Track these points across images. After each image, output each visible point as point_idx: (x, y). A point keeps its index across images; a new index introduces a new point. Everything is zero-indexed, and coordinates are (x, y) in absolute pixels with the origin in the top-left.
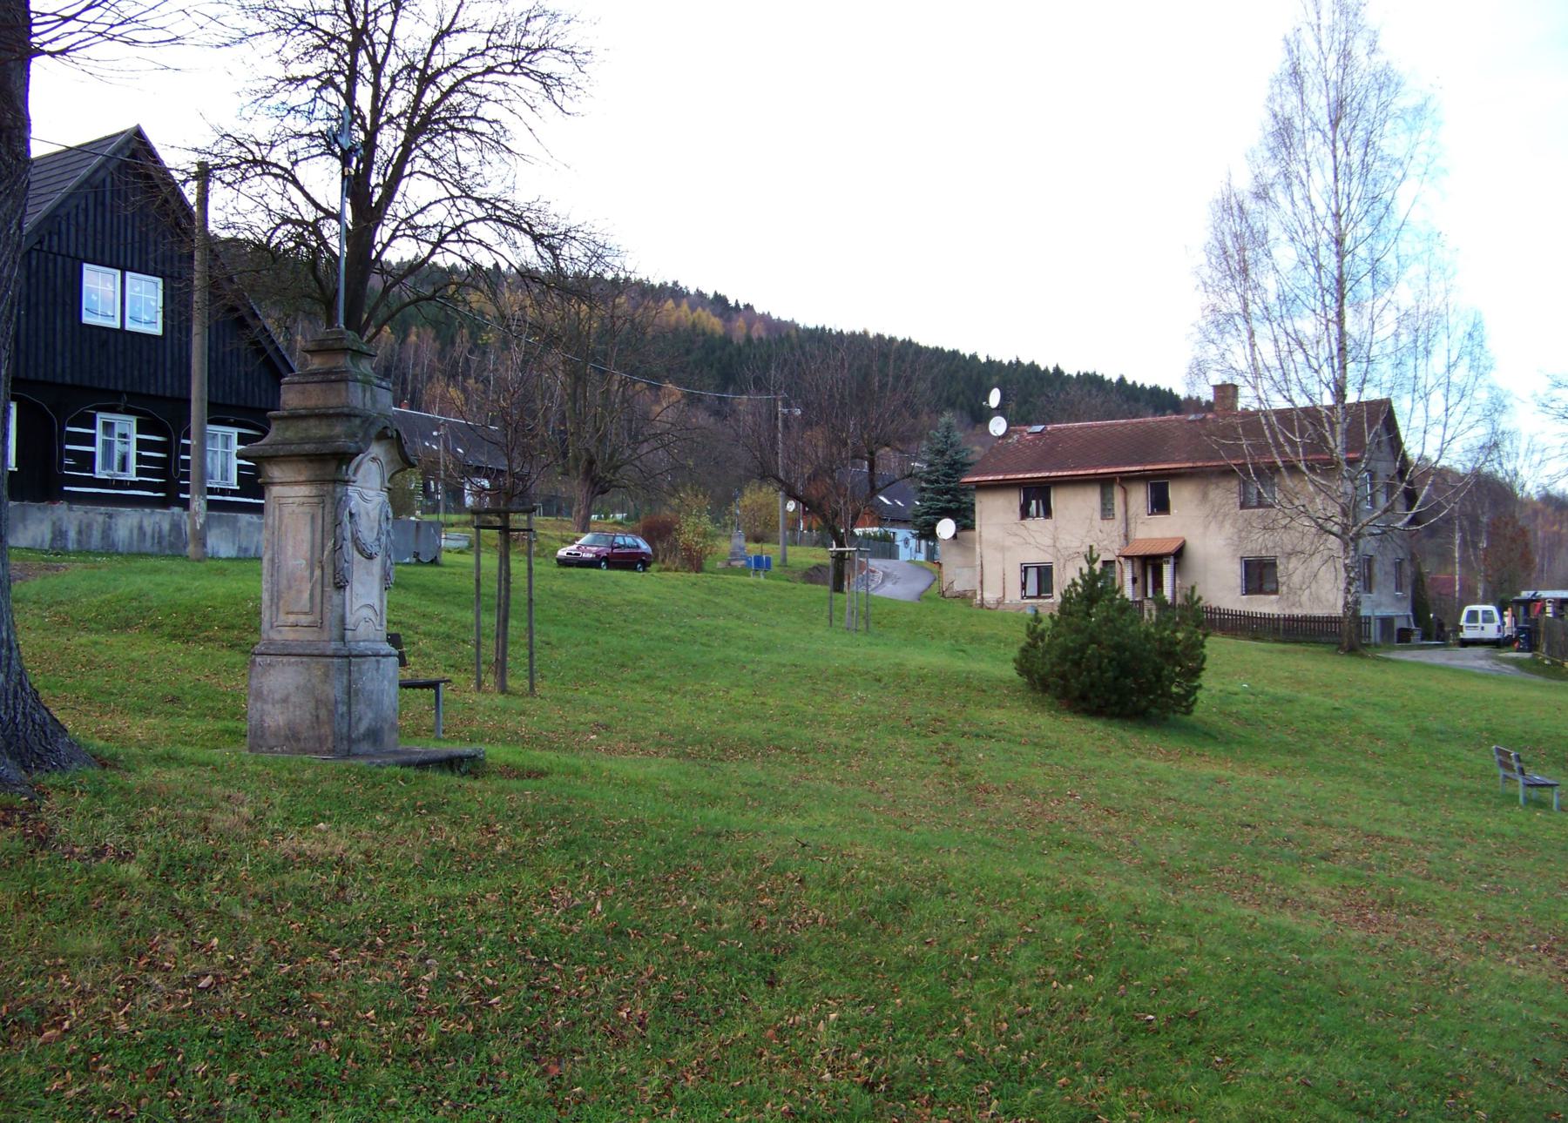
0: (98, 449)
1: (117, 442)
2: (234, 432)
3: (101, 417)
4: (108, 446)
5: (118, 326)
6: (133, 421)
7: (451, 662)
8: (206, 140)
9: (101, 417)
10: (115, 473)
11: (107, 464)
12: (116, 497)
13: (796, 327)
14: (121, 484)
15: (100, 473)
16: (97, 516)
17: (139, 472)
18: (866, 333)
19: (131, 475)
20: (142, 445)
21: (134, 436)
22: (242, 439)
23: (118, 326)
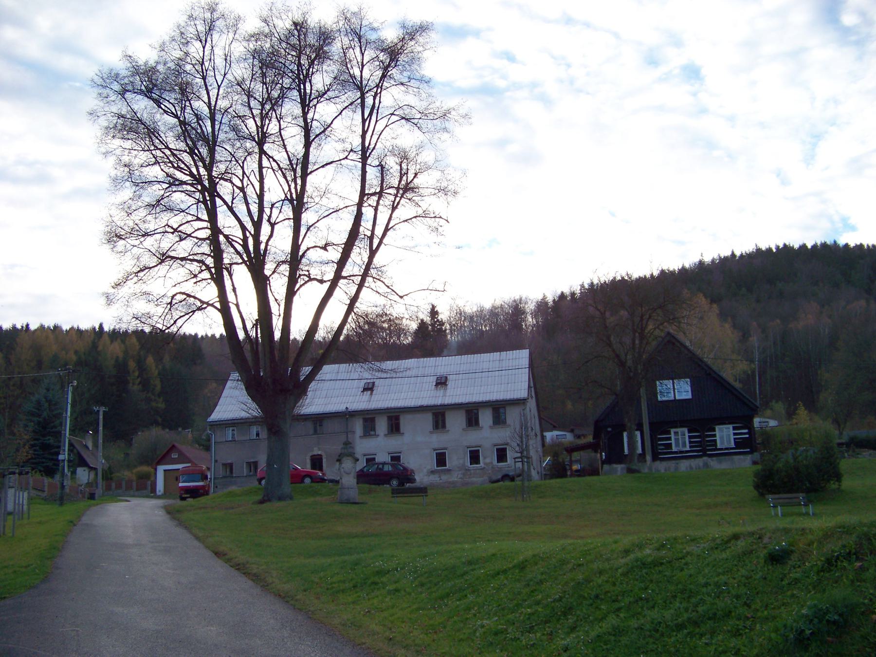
0: (673, 441)
1: (680, 438)
2: (731, 426)
3: (672, 431)
4: (677, 440)
5: (672, 398)
6: (686, 430)
7: (794, 559)
8: (624, 275)
9: (672, 431)
10: (681, 448)
11: (677, 445)
12: (682, 456)
13: (79, 332)
14: (681, 452)
15: (674, 449)
16: (672, 464)
17: (690, 447)
18: (196, 335)
19: (688, 448)
20: (690, 437)
21: (687, 435)
22: (734, 428)
23: (218, 329)
